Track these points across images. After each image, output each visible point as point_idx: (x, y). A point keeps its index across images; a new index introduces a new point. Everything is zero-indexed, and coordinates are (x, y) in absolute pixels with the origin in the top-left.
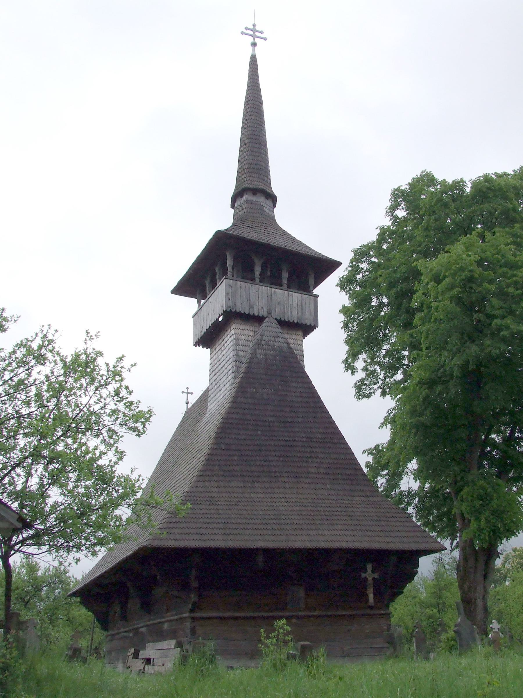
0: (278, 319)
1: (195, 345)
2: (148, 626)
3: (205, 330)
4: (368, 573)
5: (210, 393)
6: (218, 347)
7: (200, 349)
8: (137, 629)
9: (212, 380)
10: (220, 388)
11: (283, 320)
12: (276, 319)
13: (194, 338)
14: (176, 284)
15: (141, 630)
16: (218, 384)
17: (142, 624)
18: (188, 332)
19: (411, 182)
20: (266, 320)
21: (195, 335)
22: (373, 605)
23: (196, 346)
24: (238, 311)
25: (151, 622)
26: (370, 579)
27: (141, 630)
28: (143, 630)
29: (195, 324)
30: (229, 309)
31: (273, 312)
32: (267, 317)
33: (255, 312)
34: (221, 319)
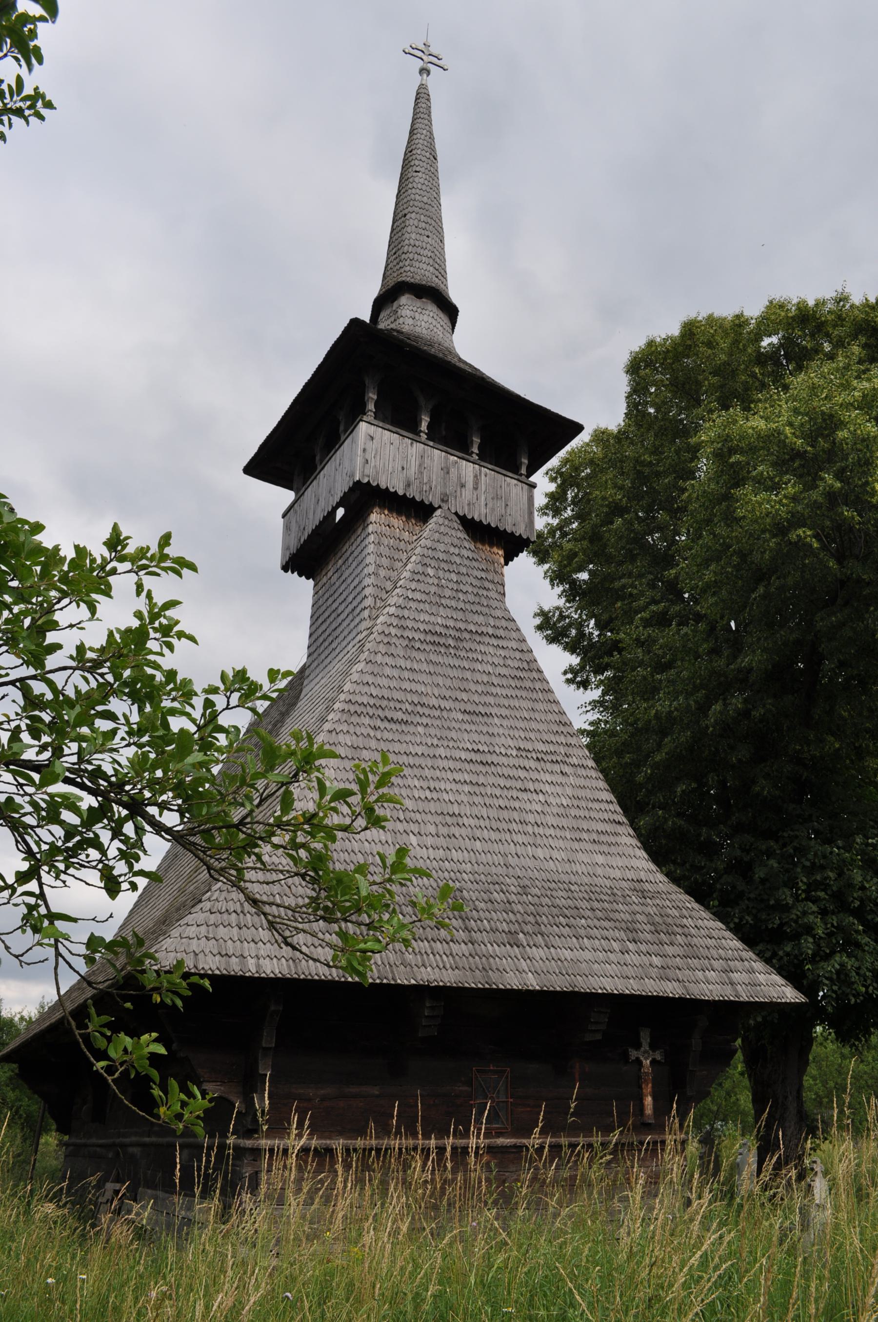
0: (461, 514)
1: (285, 568)
2: (143, 1145)
3: (309, 530)
4: (642, 1049)
5: (307, 673)
6: (330, 573)
7: (293, 578)
8: (124, 1146)
9: (315, 636)
10: (334, 645)
11: (469, 517)
12: (456, 514)
13: (283, 555)
14: (340, 333)
15: (131, 1150)
16: (330, 638)
17: (134, 1139)
18: (273, 545)
19: (811, 303)
20: (438, 512)
21: (286, 548)
22: (652, 1121)
23: (286, 571)
24: (383, 486)
25: (154, 1139)
26: (645, 1046)
27: (131, 1150)
28: (135, 1150)
29: (287, 528)
30: (365, 481)
31: (452, 500)
32: (440, 507)
33: (413, 493)
34: (340, 512)
